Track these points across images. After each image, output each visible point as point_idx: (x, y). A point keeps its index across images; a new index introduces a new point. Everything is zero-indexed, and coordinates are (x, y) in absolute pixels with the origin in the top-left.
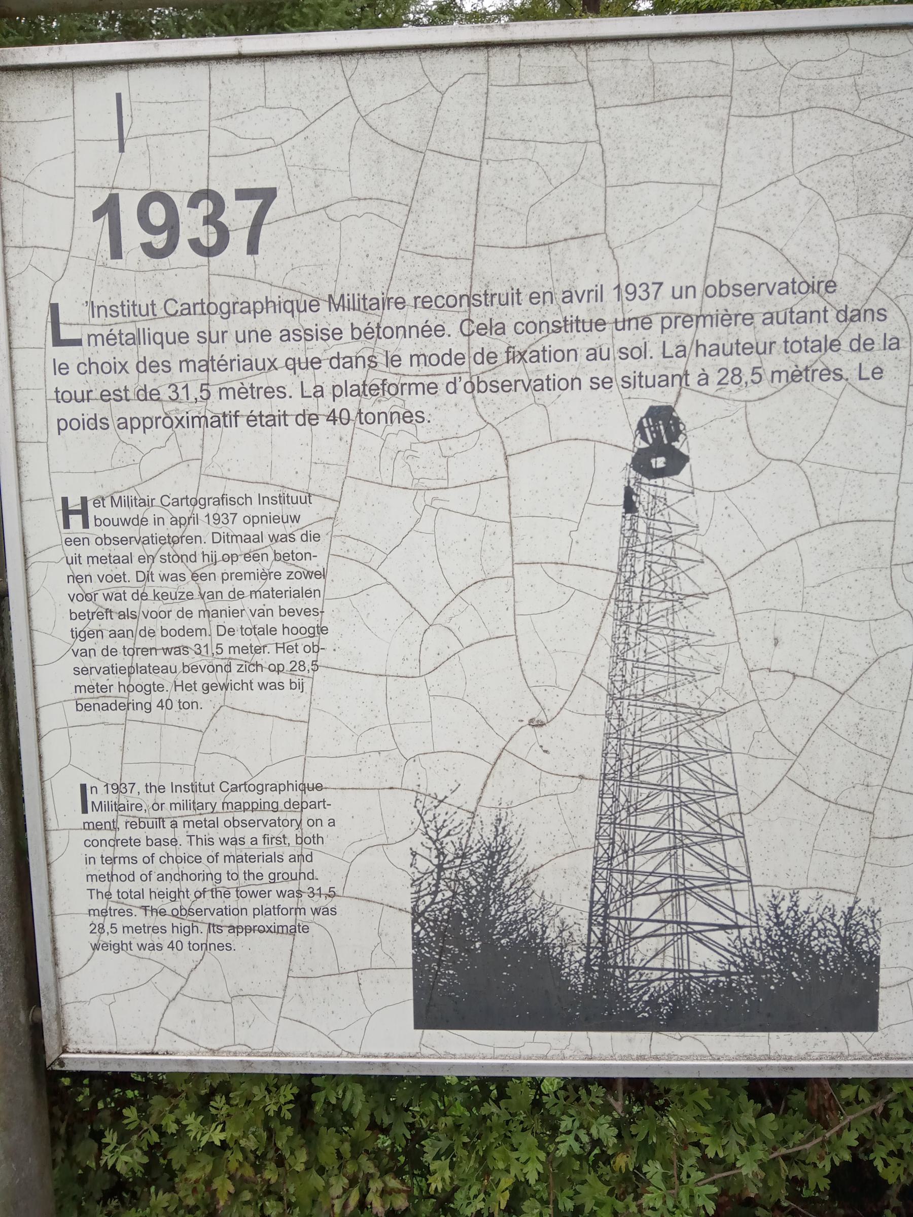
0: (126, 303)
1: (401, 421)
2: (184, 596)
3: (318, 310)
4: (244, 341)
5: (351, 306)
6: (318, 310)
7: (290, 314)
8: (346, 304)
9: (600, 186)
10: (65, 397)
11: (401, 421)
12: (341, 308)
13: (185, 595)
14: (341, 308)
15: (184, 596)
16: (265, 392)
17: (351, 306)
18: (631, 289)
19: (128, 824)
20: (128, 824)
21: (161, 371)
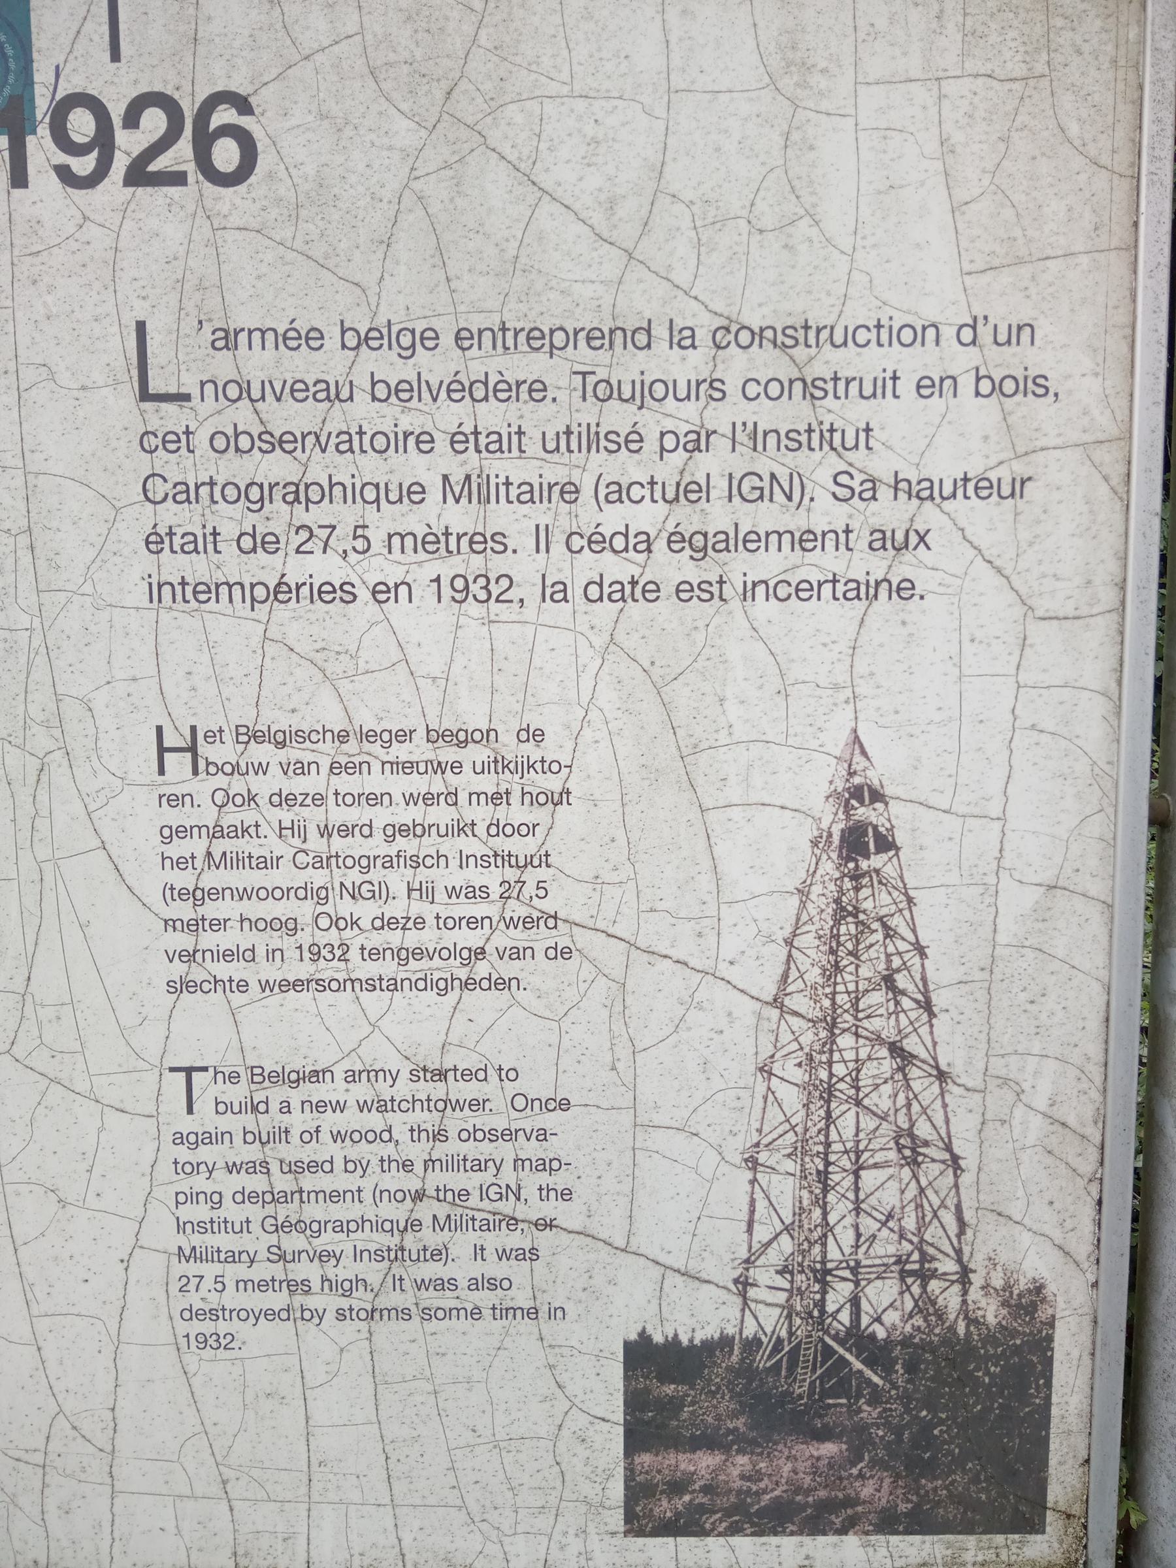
0: (575, 429)
1: (894, 595)
2: (309, 801)
3: (423, 500)
4: (240, 1112)
5: (210, 1258)
6: (423, 500)
7: (218, 978)
8: (198, 1255)
9: (399, 1478)
10: (384, 439)
11: (894, 595)
12: (192, 1260)
13: (310, 798)
14: (192, 1260)
15: (309, 801)
16: (468, 923)
17: (210, 1258)
18: (459, 584)
19: (164, 800)
20: (164, 800)
21: (338, 600)
